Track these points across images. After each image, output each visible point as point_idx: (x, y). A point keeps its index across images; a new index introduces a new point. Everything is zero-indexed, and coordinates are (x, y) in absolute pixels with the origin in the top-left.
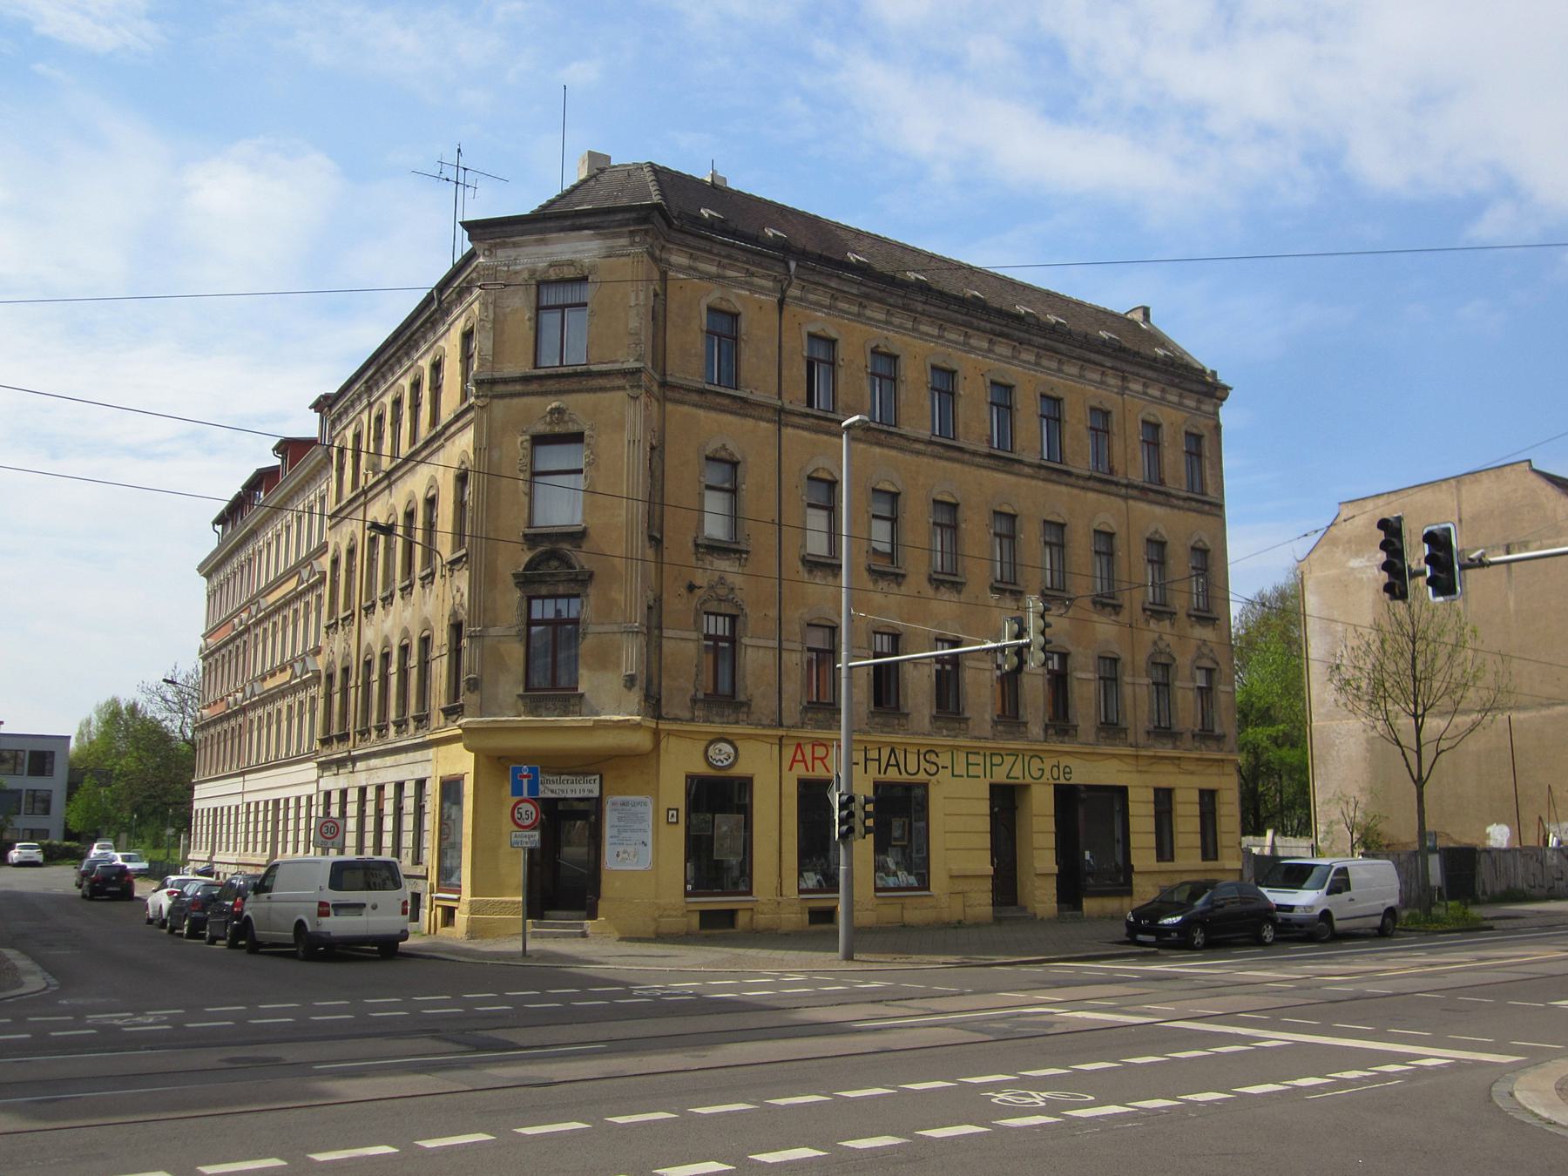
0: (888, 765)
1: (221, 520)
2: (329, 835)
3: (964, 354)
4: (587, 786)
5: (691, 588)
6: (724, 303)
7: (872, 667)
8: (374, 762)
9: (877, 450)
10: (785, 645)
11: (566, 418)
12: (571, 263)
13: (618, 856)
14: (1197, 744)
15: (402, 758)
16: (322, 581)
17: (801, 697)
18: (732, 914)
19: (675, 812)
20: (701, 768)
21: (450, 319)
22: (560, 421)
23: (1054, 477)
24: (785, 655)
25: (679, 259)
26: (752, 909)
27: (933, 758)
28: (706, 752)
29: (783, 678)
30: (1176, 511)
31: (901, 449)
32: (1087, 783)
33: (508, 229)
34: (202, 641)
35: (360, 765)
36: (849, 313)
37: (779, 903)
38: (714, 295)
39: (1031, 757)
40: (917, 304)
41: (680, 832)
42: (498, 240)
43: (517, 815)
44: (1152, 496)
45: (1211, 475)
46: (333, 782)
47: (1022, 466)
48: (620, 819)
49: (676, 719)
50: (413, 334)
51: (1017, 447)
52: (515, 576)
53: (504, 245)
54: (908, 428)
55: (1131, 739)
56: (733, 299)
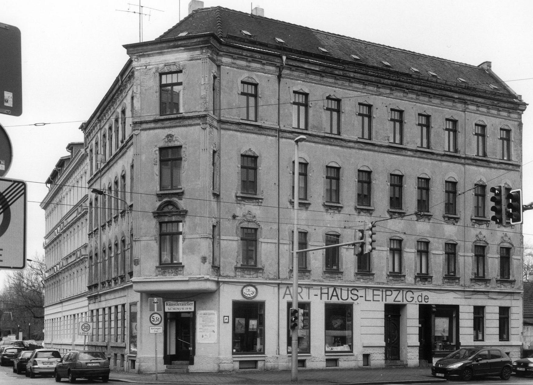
0: (332, 296)
1: (49, 181)
2: (86, 330)
3: (376, 97)
4: (189, 307)
5: (234, 217)
6: (250, 79)
7: (325, 250)
8: (108, 297)
9: (329, 147)
10: (281, 241)
11: (174, 139)
12: (174, 64)
13: (203, 337)
14: (499, 285)
15: (117, 295)
16: (86, 213)
17: (289, 265)
18: (256, 362)
19: (227, 318)
20: (239, 298)
21: (127, 90)
22: (170, 141)
23: (424, 156)
24: (281, 246)
25: (225, 60)
26: (264, 360)
27: (355, 292)
28: (242, 291)
29: (280, 257)
30: (493, 170)
31: (342, 146)
32: (437, 304)
33: (145, 48)
34: (44, 241)
35: (103, 298)
36: (315, 80)
37: (277, 358)
38: (245, 75)
39: (407, 292)
40: (350, 73)
41: (229, 327)
42: (141, 54)
43: (152, 320)
44: (479, 163)
45: (515, 150)
46: (93, 307)
47: (406, 151)
48: (203, 321)
49: (227, 276)
50: (113, 96)
51: (405, 142)
52: (154, 213)
53: (143, 56)
54: (346, 136)
55: (462, 282)
56: (254, 77)
